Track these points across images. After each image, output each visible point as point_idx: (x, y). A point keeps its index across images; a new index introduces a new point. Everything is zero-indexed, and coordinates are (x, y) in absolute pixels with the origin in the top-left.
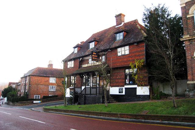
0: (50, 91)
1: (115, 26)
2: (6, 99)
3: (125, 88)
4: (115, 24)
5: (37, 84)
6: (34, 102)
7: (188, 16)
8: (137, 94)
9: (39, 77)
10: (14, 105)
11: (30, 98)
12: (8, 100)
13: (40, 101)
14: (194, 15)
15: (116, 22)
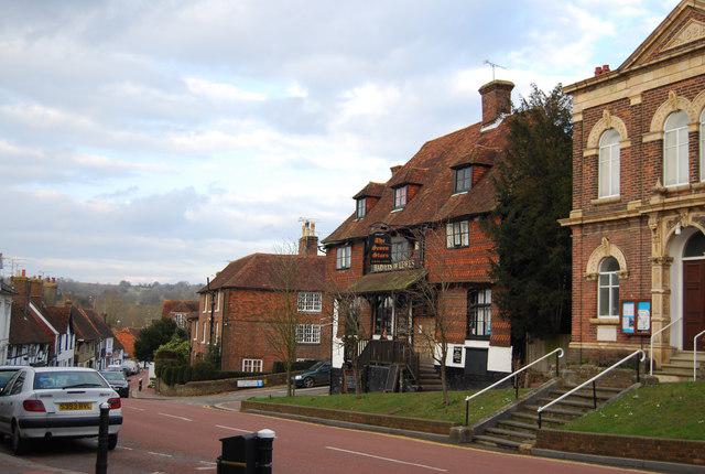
0: (300, 344)
1: (478, 126)
2: (152, 367)
3: (467, 349)
4: (479, 118)
5: (253, 318)
6: (240, 383)
7: (585, 154)
8: (489, 369)
9: (259, 294)
10: (175, 395)
11: (225, 369)
12: (158, 371)
13: (260, 381)
14: (600, 153)
15: (481, 110)
